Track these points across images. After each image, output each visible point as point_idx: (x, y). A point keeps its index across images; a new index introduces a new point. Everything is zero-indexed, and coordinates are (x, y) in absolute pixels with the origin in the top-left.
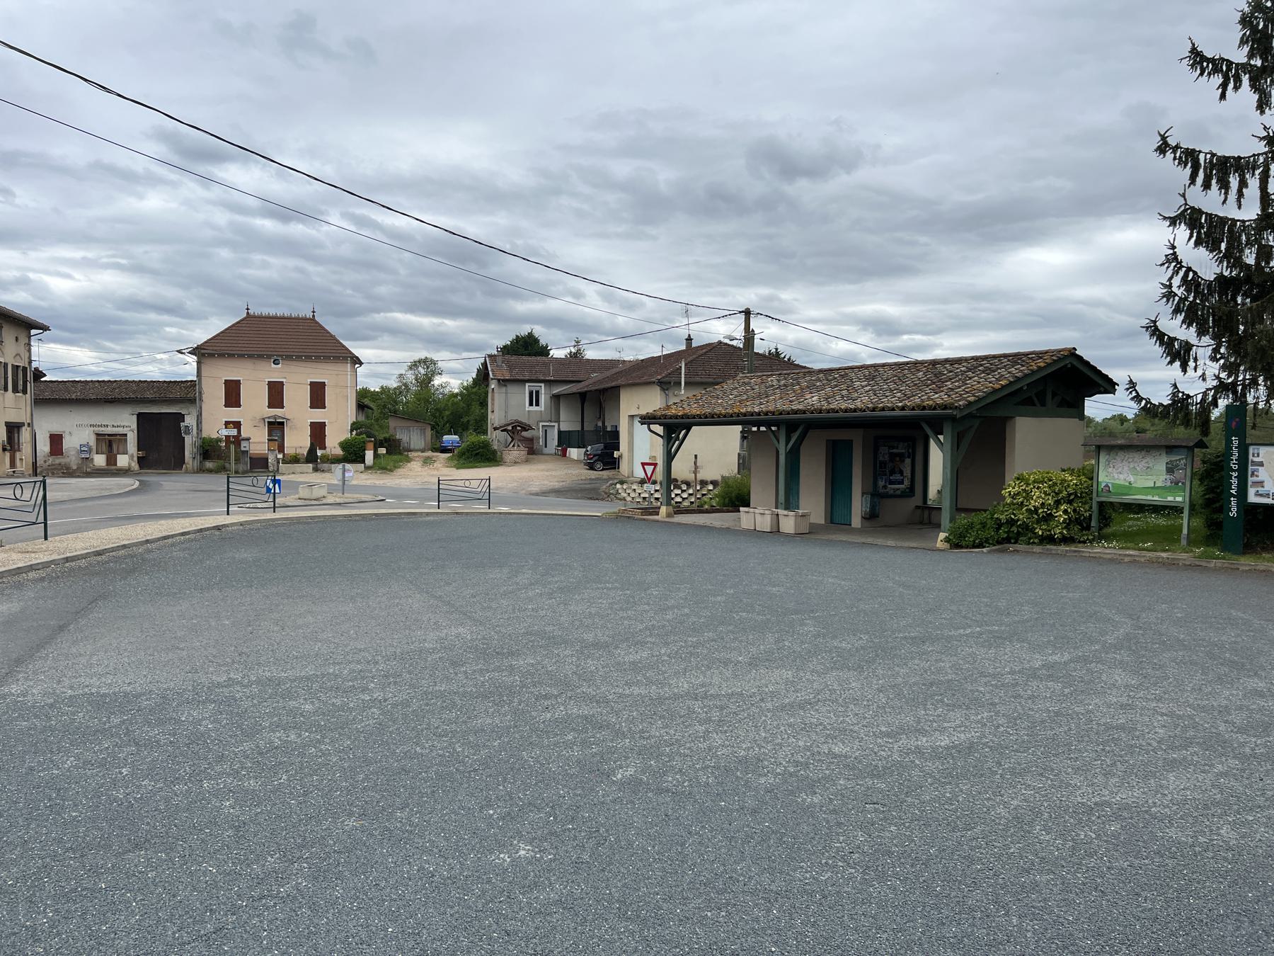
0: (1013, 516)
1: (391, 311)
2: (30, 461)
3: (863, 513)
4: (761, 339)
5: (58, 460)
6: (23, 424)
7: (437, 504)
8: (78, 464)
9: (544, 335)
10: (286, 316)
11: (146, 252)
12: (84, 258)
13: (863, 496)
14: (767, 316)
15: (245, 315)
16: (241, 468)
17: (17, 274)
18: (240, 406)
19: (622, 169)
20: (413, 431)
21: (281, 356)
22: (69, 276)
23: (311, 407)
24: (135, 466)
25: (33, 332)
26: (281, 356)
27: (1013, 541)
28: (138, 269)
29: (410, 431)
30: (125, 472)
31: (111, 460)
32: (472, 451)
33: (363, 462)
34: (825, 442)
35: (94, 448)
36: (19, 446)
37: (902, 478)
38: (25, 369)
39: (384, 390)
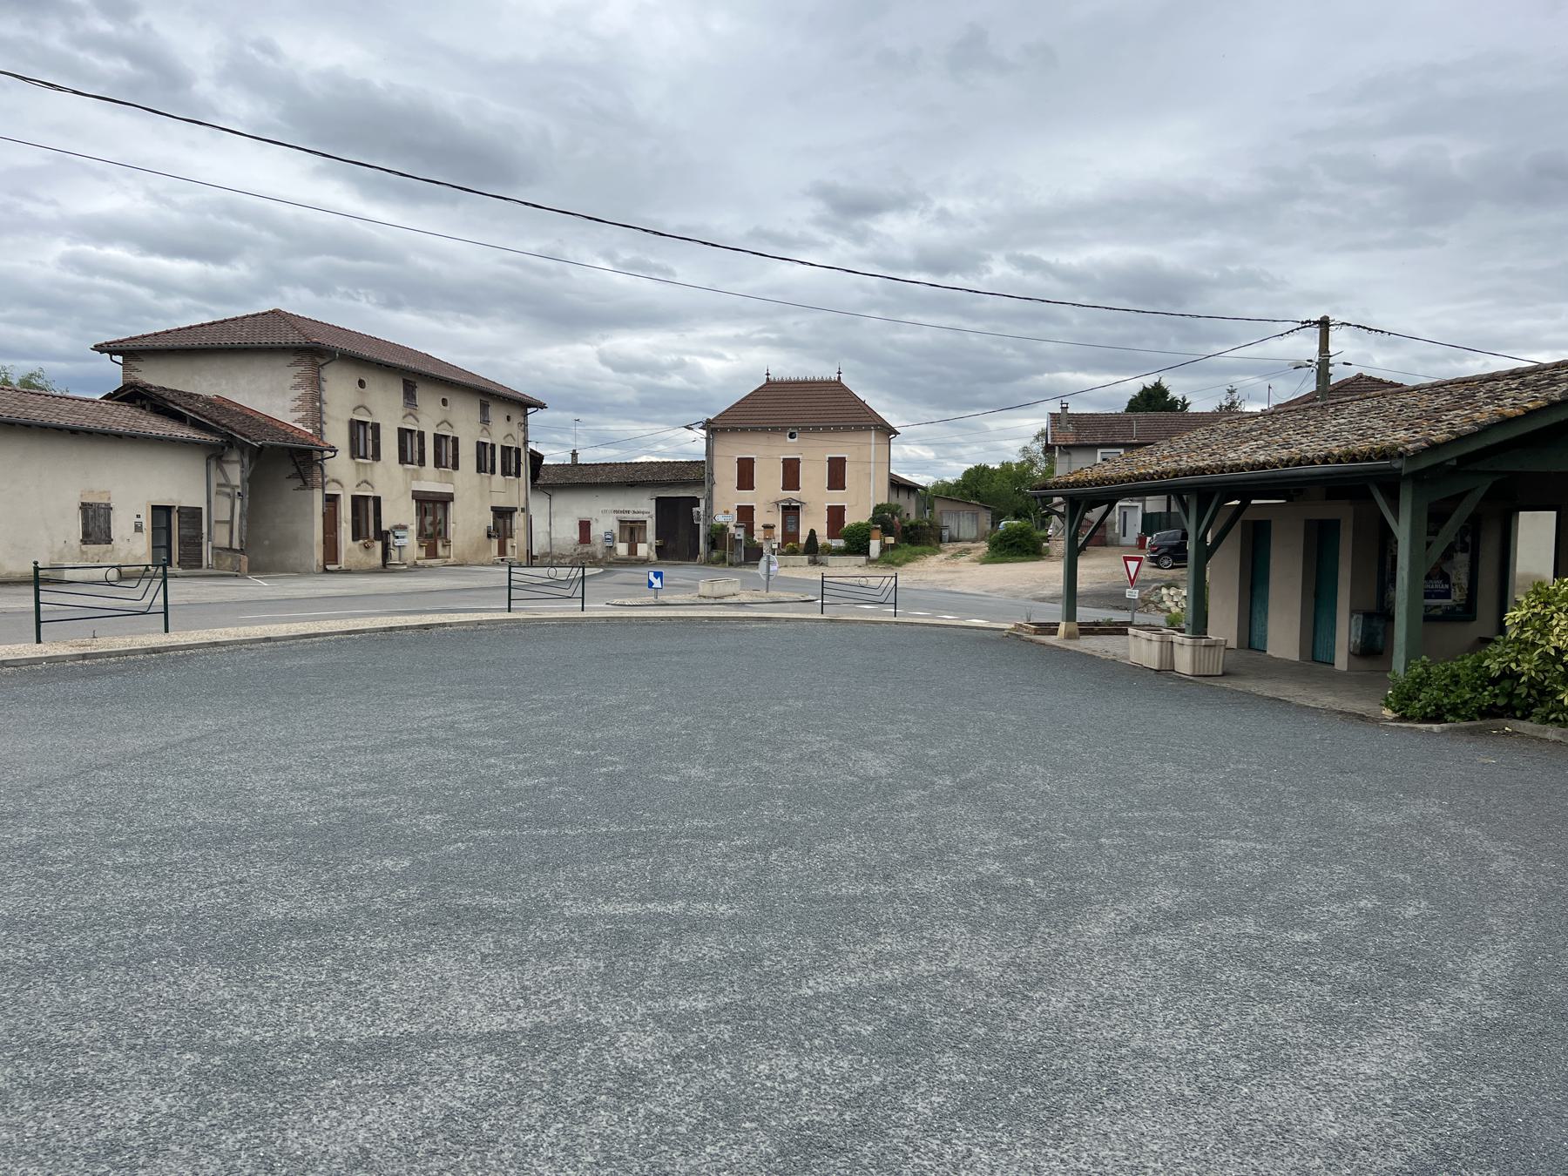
0: (1513, 665)
1: (1058, 370)
2: (524, 548)
3: (1352, 645)
4: (1345, 363)
5: (588, 549)
6: (516, 509)
7: (893, 610)
8: (603, 553)
9: (1176, 387)
10: (800, 379)
11: (796, 324)
12: (737, 336)
13: (1351, 616)
14: (1359, 326)
15: (765, 382)
16: (735, 559)
17: (674, 357)
18: (752, 488)
19: (1391, 152)
20: (963, 516)
21: (797, 428)
22: (720, 357)
23: (829, 488)
24: (654, 556)
25: (529, 410)
26: (797, 428)
27: (1518, 714)
28: (786, 343)
29: (959, 516)
30: (644, 562)
31: (633, 550)
32: (1006, 541)
33: (867, 553)
34: (1303, 524)
35: (617, 536)
36: (511, 532)
37: (1447, 586)
38: (518, 451)
39: (1006, 466)
